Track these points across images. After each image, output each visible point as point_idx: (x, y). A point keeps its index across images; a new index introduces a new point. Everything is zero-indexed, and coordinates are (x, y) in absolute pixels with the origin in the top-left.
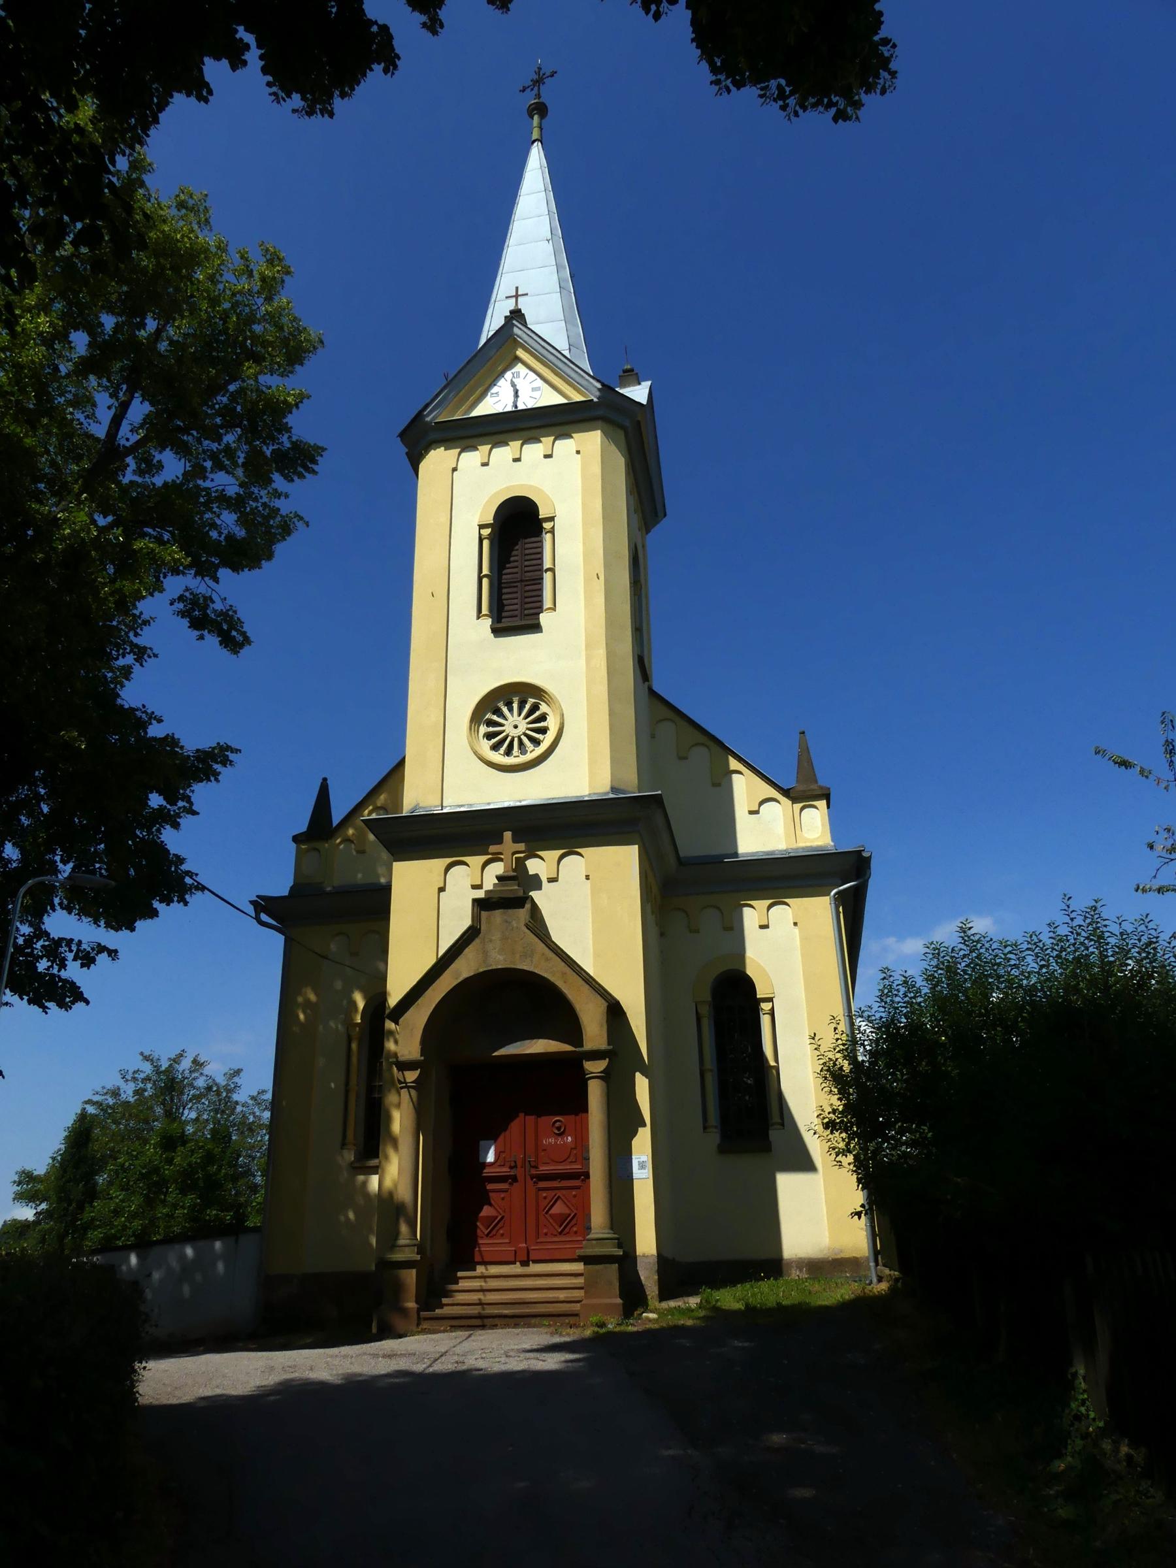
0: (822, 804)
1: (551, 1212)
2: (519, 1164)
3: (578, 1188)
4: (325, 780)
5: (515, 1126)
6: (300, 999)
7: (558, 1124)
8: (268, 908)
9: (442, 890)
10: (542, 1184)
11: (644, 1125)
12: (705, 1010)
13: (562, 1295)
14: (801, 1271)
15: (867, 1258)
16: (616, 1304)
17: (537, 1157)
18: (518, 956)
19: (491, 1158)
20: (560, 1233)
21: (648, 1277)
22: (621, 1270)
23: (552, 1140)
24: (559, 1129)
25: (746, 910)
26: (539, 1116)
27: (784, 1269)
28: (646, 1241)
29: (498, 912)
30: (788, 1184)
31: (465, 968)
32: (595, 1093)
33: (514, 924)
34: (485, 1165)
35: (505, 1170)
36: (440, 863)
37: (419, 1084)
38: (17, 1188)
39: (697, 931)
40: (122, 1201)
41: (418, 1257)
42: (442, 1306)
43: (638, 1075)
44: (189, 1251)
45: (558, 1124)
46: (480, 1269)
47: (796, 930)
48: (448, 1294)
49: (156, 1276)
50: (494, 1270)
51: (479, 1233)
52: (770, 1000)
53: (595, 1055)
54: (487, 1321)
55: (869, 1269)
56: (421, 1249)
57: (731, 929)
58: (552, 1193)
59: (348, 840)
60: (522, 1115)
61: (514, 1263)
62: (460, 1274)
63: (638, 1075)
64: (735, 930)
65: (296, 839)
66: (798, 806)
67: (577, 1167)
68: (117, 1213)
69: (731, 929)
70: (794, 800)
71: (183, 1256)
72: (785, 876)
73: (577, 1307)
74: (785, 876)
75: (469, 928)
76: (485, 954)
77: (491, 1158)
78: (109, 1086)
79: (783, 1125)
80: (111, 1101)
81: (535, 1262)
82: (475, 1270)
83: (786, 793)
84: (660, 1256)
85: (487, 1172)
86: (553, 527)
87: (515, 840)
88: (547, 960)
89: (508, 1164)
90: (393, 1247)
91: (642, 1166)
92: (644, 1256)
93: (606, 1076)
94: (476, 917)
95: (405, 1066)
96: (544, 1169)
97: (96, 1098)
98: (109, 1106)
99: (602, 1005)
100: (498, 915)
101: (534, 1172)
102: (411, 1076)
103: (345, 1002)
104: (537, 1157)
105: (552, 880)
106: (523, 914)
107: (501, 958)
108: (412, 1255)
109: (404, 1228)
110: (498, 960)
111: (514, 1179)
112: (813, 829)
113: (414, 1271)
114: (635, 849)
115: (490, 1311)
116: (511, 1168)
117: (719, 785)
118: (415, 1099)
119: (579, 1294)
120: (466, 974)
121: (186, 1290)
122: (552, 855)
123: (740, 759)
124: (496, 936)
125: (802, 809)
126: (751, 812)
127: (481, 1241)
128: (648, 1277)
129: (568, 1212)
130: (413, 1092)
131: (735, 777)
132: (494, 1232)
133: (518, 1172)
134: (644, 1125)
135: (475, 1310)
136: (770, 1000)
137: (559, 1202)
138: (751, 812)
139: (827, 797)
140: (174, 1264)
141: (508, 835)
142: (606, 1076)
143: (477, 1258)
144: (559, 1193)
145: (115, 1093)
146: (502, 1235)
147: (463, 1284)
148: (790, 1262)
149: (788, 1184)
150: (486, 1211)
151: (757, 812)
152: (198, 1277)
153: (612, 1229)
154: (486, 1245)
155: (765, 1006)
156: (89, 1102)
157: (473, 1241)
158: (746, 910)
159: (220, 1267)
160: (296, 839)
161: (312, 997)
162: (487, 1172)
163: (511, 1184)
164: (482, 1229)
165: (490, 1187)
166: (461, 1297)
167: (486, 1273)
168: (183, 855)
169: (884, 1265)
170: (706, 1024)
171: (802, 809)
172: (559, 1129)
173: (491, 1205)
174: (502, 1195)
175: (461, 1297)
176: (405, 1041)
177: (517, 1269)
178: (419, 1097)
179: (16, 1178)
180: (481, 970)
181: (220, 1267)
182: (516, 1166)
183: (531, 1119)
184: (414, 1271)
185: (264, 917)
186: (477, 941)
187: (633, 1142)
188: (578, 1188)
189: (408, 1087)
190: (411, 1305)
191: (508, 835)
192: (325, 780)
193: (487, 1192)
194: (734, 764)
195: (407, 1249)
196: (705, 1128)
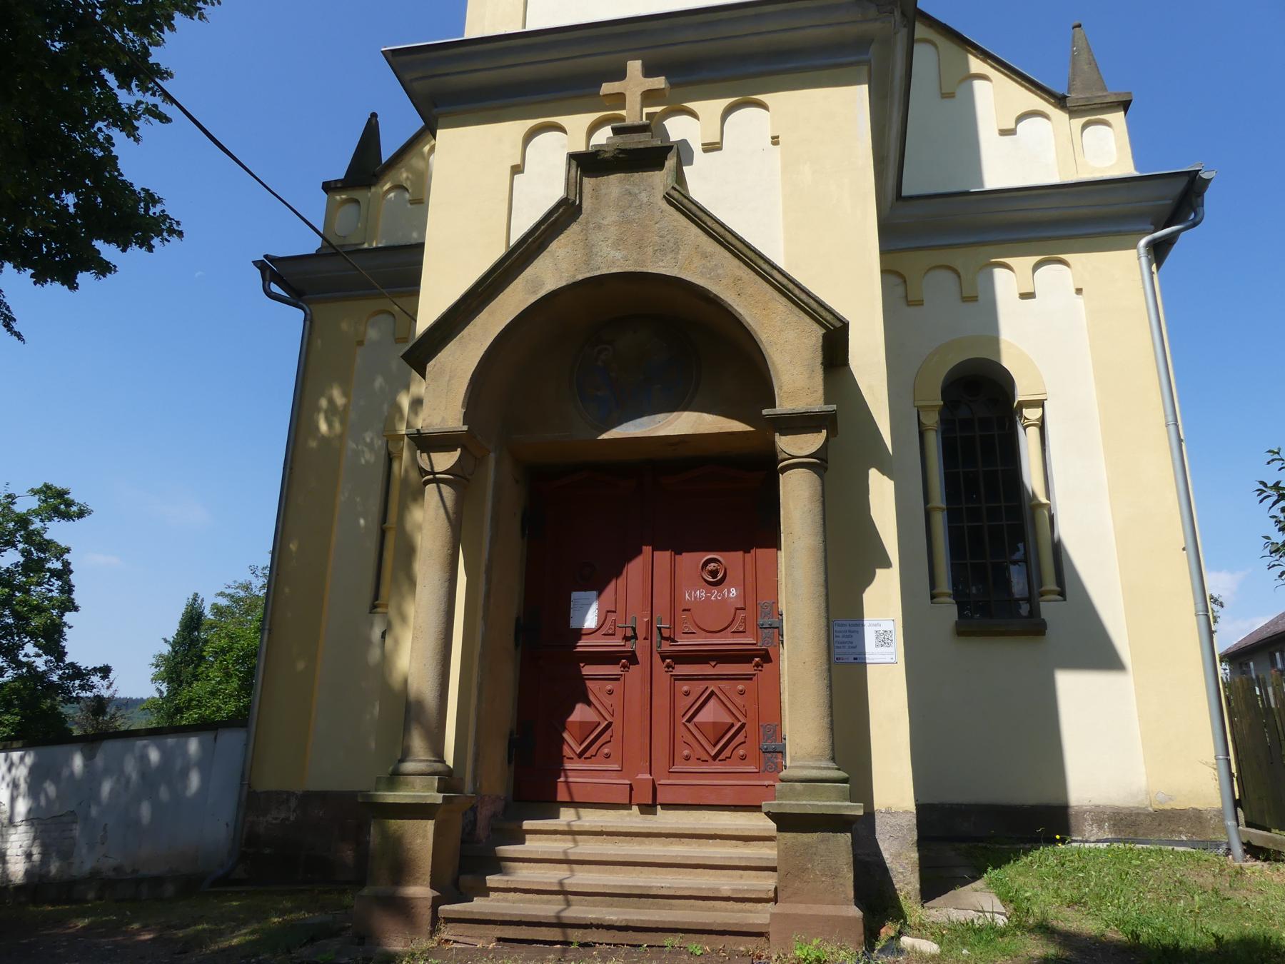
0: (1118, 118)
1: (696, 720)
2: (641, 633)
3: (748, 678)
4: (374, 115)
5: (635, 569)
6: (324, 403)
7: (712, 566)
8: (284, 277)
9: (517, 170)
10: (682, 669)
11: (888, 564)
12: (932, 420)
13: (725, 883)
14: (1100, 827)
15: (1220, 814)
16: (849, 919)
17: (673, 622)
18: (650, 250)
19: (591, 621)
20: (714, 758)
21: (900, 856)
22: (855, 844)
23: (701, 594)
24: (714, 573)
25: (999, 273)
26: (678, 551)
27: (1073, 821)
28: (894, 787)
29: (614, 179)
30: (1075, 691)
31: (551, 272)
32: (797, 497)
33: (644, 197)
34: (579, 633)
35: (615, 643)
36: (516, 129)
37: (458, 477)
38: (154, 670)
39: (920, 303)
40: (219, 683)
41: (438, 798)
42: (485, 891)
43: (874, 474)
44: (154, 755)
45: (712, 566)
46: (567, 816)
47: (1080, 300)
48: (497, 865)
49: (106, 787)
50: (592, 819)
51: (567, 751)
52: (1040, 404)
53: (800, 423)
54: (576, 935)
55: (1225, 830)
56: (448, 781)
57: (974, 299)
58: (700, 686)
59: (399, 187)
60: (647, 550)
61: (627, 807)
62: (527, 825)
63: (874, 474)
64: (980, 302)
65: (328, 187)
66: (1080, 122)
67: (747, 640)
68: (213, 694)
69: (974, 299)
70: (1074, 113)
71: (144, 758)
72: (1061, 219)
73: (759, 916)
74: (1061, 219)
75: (562, 203)
76: (589, 250)
77: (591, 621)
78: (242, 580)
79: (1062, 594)
80: (242, 594)
81: (667, 806)
82: (556, 816)
83: (1060, 101)
84: (924, 810)
85: (584, 644)
86: (1042, 419)
87: (648, 72)
88: (705, 256)
89: (620, 634)
90: (395, 778)
91: (884, 639)
92: (888, 812)
93: (819, 464)
94: (573, 185)
95: (428, 442)
96: (685, 642)
97: (227, 591)
98: (241, 599)
99: (813, 335)
100: (614, 184)
101: (666, 646)
102: (444, 461)
103: (385, 407)
104: (673, 622)
105: (711, 147)
106: (660, 180)
107: (618, 255)
108: (424, 791)
109: (418, 743)
110: (612, 258)
111: (632, 658)
112: (1105, 151)
113: (430, 825)
114: (864, 89)
115: (580, 911)
116: (626, 639)
117: (951, 95)
118: (449, 503)
119: (767, 883)
120: (551, 283)
121: (145, 810)
122: (710, 108)
123: (986, 56)
124: (611, 217)
125: (1085, 126)
126: (1003, 132)
127: (568, 766)
128: (900, 856)
129: (729, 720)
130: (447, 491)
131: (977, 84)
132: (592, 751)
133: (640, 647)
134: (888, 564)
135: (547, 908)
136: (1040, 404)
137: (712, 702)
138: (1003, 132)
139: (1125, 105)
140: (131, 767)
141: (635, 67)
142: (819, 464)
143: (562, 795)
144: (713, 686)
145: (247, 587)
146: (608, 756)
147: (533, 846)
148: (1082, 813)
149: (1075, 691)
150: (580, 713)
151: (1012, 132)
152: (164, 794)
153: (833, 759)
154: (578, 773)
155: (1032, 414)
156: (222, 594)
157: (556, 767)
158: (999, 273)
159: (195, 780)
160: (328, 187)
161: (340, 400)
162: (584, 644)
163: (624, 666)
164: (571, 744)
165: (587, 670)
166: (525, 875)
167: (577, 826)
168: (171, 206)
169: (1249, 824)
170: (934, 441)
171: (1085, 126)
172: (714, 573)
173: (589, 703)
174: (609, 686)
175: (525, 875)
176: (440, 398)
177: (632, 819)
178: (459, 501)
179: (154, 661)
180: (580, 277)
181: (195, 780)
182: (635, 637)
183: (663, 557)
184: (430, 825)
185: (275, 288)
186: (574, 227)
187: (865, 596)
188: (748, 678)
189: (437, 481)
190: (420, 891)
191: (635, 67)
192: (374, 115)
193: (583, 679)
194: (976, 65)
195: (418, 780)
196: (933, 597)
